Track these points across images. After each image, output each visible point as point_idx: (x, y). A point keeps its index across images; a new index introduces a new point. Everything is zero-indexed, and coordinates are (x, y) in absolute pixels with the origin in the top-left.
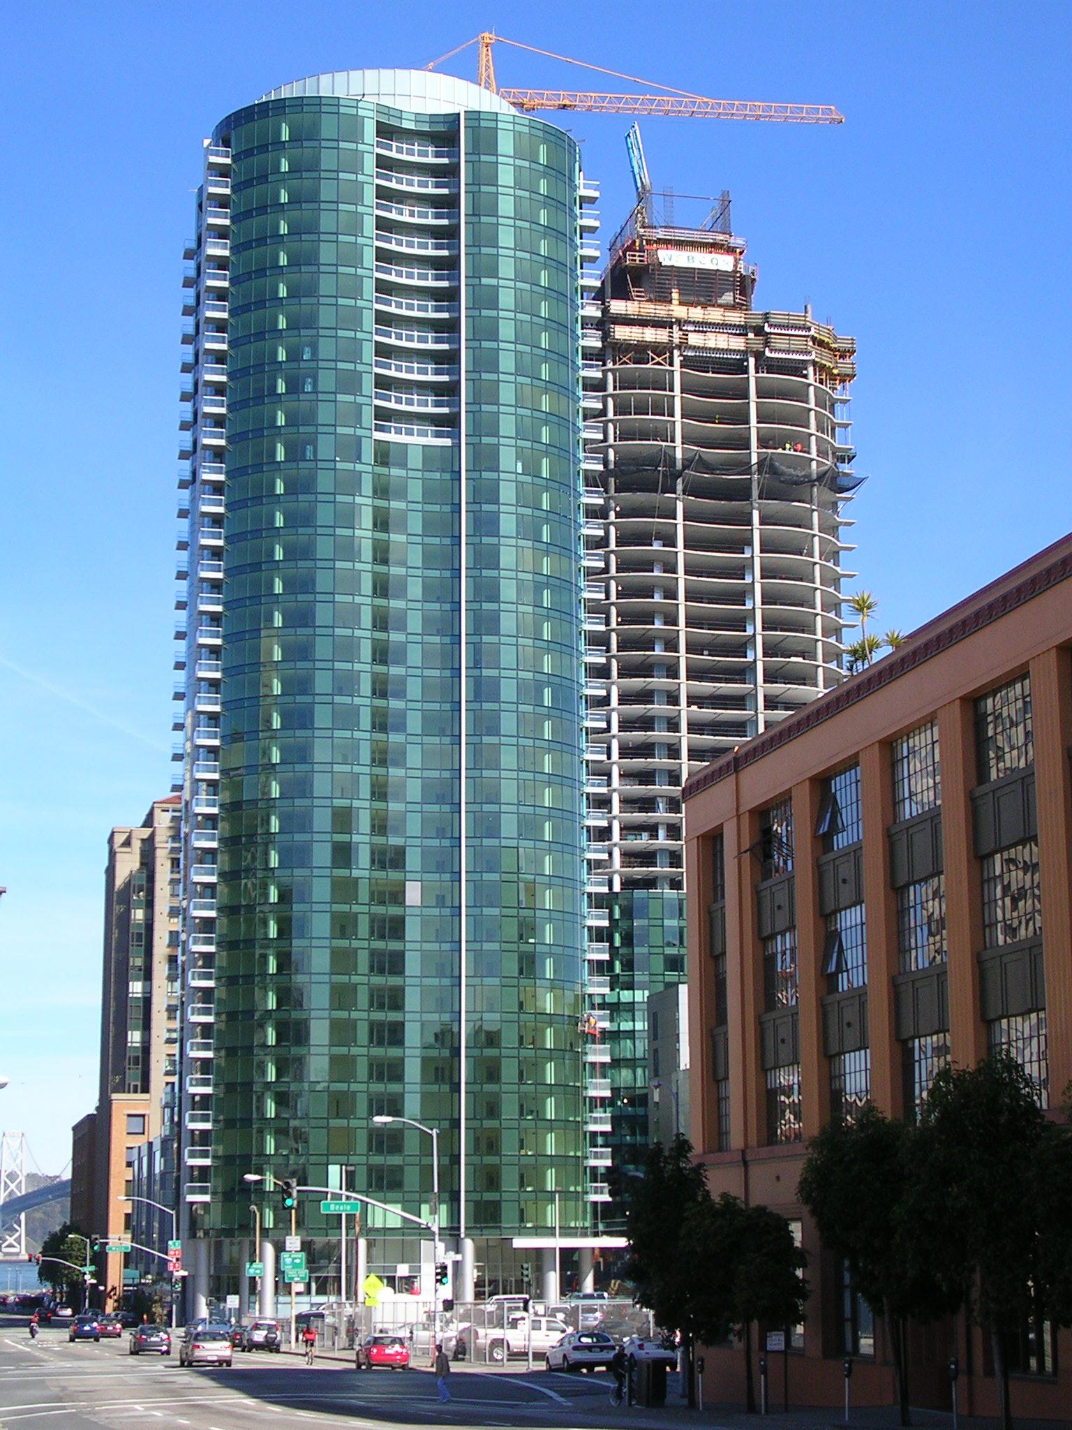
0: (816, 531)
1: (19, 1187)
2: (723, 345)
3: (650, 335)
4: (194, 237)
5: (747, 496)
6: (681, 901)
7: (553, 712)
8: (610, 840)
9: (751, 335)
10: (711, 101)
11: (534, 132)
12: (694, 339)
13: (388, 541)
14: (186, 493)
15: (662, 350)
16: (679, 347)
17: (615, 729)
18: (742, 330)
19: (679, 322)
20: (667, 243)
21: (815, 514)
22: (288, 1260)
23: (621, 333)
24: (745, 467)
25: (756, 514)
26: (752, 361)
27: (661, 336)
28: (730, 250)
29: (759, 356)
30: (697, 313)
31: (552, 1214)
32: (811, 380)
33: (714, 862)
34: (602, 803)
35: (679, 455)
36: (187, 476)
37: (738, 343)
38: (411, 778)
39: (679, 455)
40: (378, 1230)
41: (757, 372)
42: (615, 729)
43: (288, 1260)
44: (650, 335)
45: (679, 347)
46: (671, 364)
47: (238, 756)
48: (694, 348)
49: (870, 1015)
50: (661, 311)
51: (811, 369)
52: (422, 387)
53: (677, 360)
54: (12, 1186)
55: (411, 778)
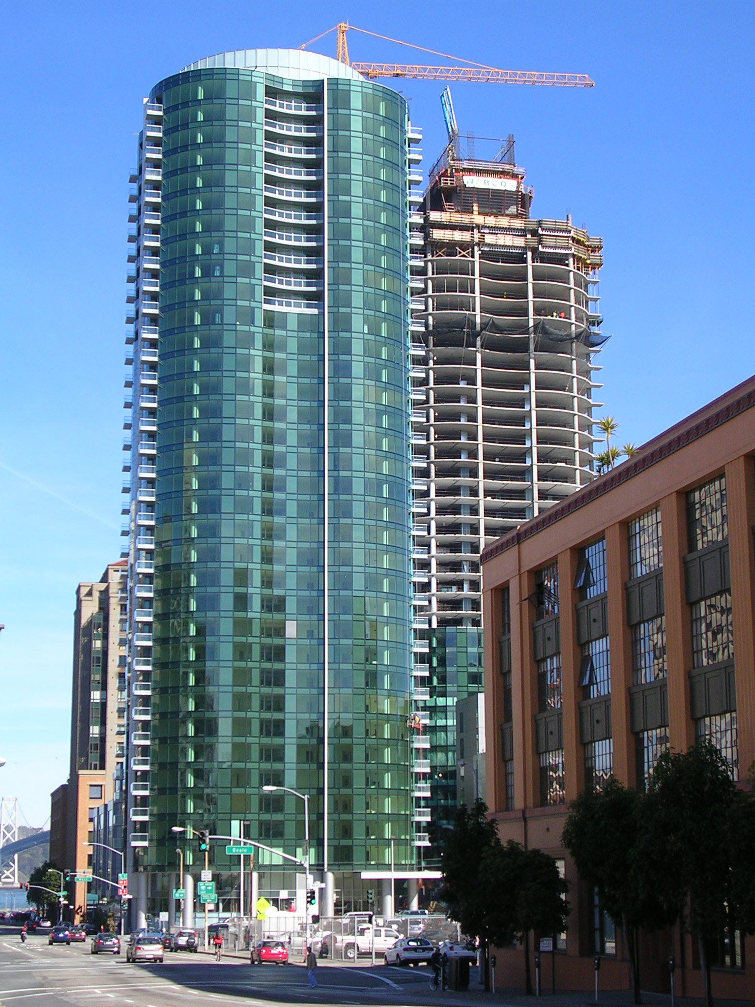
0: (575, 374)
1: (13, 836)
2: (509, 243)
3: (458, 236)
4: (137, 167)
5: (526, 349)
6: (479, 634)
7: (390, 501)
8: (430, 591)
9: (529, 236)
10: (501, 71)
11: (376, 93)
12: (489, 239)
13: (273, 381)
14: (131, 347)
15: (466, 246)
16: (478, 244)
17: (433, 513)
18: (523, 233)
19: (478, 227)
20: (470, 171)
21: (574, 362)
22: (203, 888)
23: (438, 234)
24: (525, 329)
25: (532, 362)
26: (529, 254)
27: (466, 236)
28: (514, 176)
29: (534, 250)
30: (491, 221)
31: (389, 855)
32: (571, 268)
33: (503, 607)
34: (424, 565)
35: (478, 320)
36: (132, 335)
37: (520, 242)
38: (289, 548)
39: (478, 320)
40: (266, 866)
41: (533, 262)
42: (433, 513)
43: (203, 888)
44: (458, 236)
45: (478, 244)
46: (473, 257)
47: (168, 532)
48: (489, 245)
49: (612, 715)
50: (465, 219)
51: (571, 260)
52: (297, 272)
53: (477, 254)
54: (9, 835)
55: (289, 548)
